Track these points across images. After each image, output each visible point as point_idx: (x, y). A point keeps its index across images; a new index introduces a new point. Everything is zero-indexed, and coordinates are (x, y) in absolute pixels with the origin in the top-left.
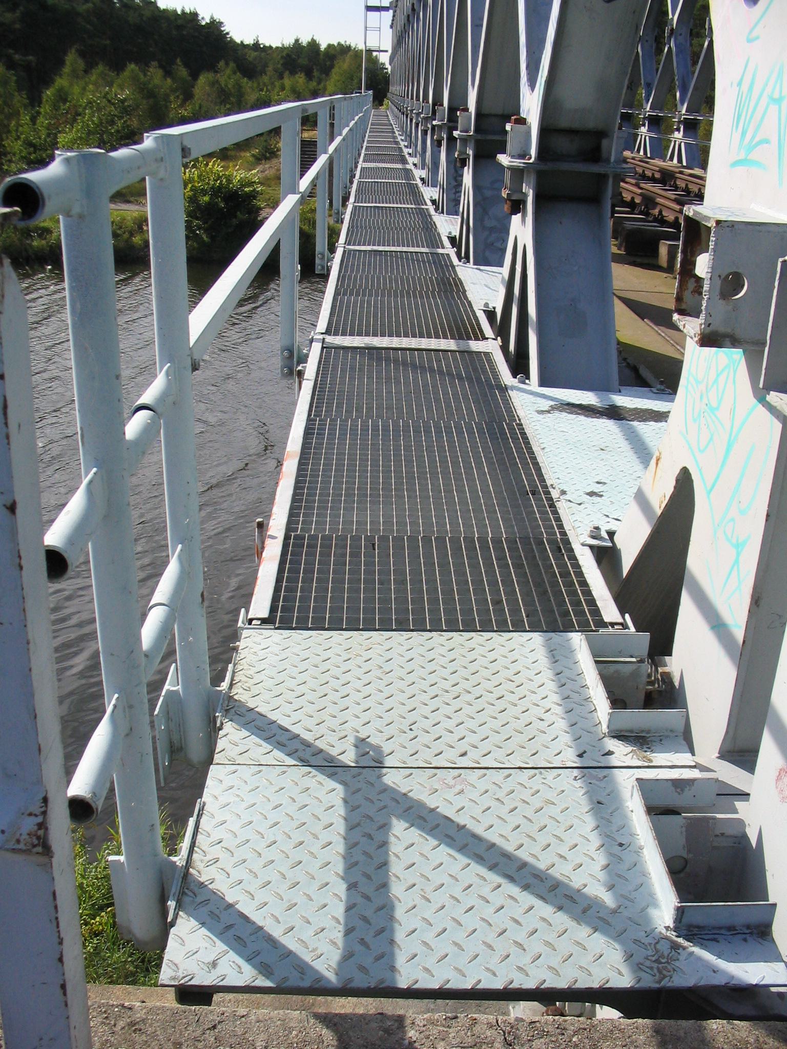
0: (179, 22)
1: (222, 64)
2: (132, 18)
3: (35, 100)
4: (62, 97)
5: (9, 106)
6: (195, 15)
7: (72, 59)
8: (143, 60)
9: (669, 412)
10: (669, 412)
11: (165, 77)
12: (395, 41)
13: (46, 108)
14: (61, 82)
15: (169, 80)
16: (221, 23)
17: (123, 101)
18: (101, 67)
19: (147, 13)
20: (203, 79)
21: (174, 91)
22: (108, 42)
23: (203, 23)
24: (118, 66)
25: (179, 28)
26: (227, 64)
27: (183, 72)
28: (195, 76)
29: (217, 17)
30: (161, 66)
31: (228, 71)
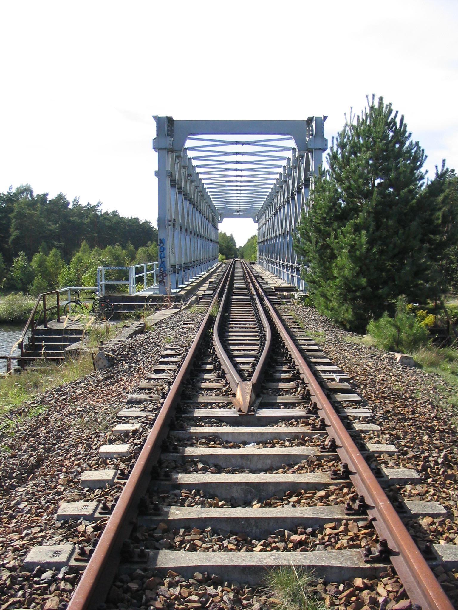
0: (130, 223)
1: (150, 242)
2: (107, 223)
3: (68, 262)
4: (80, 260)
5: (57, 265)
6: (138, 219)
7: (84, 244)
8: (112, 242)
9: (156, 118)
10: (156, 118)
11: (122, 250)
12: (383, 472)
13: (72, 265)
14: (79, 254)
15: (124, 251)
16: (150, 222)
17: (105, 262)
18: (96, 248)
19: (114, 220)
20: (140, 250)
21: (127, 256)
22: (96, 235)
23: (141, 223)
24: (104, 247)
25: (130, 226)
26: (152, 243)
27: (132, 247)
28: (137, 249)
29: (148, 220)
30: (121, 245)
31: (152, 246)
